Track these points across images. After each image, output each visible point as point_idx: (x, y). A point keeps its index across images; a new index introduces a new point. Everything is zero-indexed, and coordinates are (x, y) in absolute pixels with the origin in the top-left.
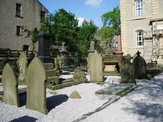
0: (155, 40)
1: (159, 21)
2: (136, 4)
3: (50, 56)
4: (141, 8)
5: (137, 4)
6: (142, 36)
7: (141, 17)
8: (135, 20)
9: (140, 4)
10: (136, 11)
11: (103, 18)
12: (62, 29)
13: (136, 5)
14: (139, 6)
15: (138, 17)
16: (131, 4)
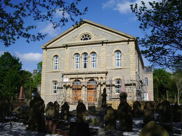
0: (64, 90)
1: (67, 74)
2: (54, 59)
3: (64, 119)
4: (95, 60)
5: (117, 55)
6: (56, 86)
7: (120, 67)
8: (115, 69)
9: (78, 58)
10: (75, 63)
11: (38, 66)
12: (3, 72)
13: (116, 56)
14: (56, 62)
15: (76, 68)
16: (50, 60)
